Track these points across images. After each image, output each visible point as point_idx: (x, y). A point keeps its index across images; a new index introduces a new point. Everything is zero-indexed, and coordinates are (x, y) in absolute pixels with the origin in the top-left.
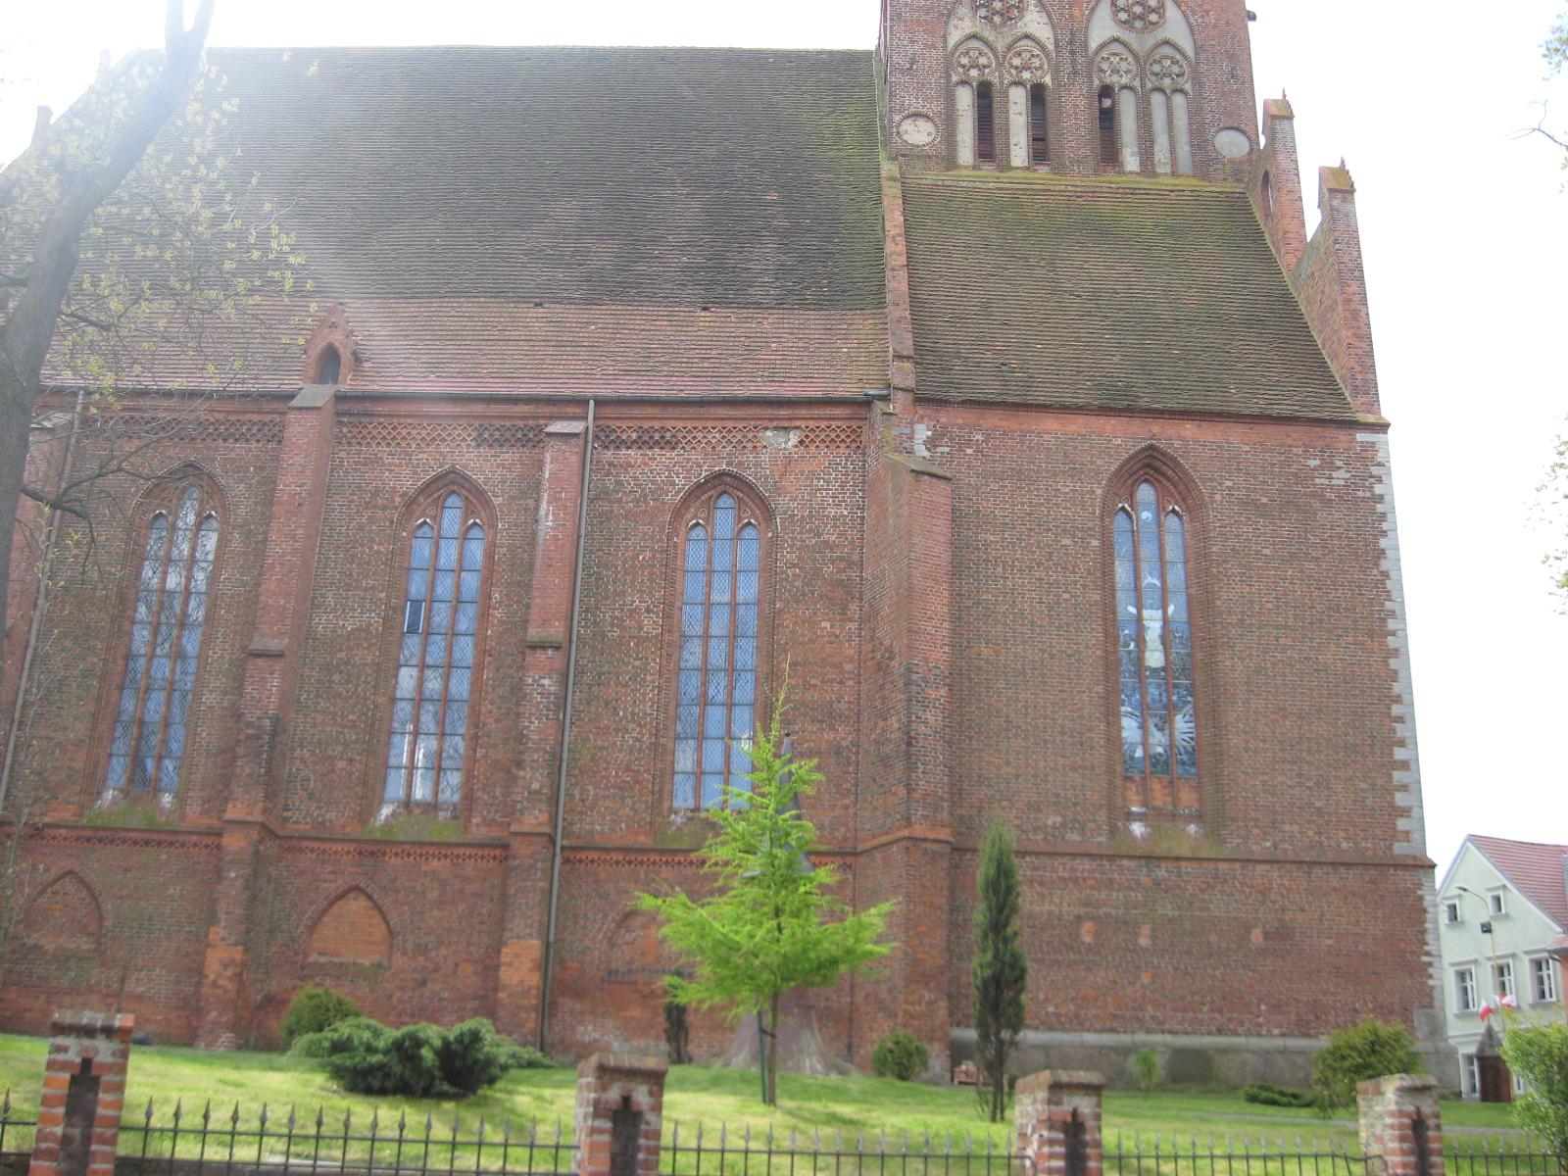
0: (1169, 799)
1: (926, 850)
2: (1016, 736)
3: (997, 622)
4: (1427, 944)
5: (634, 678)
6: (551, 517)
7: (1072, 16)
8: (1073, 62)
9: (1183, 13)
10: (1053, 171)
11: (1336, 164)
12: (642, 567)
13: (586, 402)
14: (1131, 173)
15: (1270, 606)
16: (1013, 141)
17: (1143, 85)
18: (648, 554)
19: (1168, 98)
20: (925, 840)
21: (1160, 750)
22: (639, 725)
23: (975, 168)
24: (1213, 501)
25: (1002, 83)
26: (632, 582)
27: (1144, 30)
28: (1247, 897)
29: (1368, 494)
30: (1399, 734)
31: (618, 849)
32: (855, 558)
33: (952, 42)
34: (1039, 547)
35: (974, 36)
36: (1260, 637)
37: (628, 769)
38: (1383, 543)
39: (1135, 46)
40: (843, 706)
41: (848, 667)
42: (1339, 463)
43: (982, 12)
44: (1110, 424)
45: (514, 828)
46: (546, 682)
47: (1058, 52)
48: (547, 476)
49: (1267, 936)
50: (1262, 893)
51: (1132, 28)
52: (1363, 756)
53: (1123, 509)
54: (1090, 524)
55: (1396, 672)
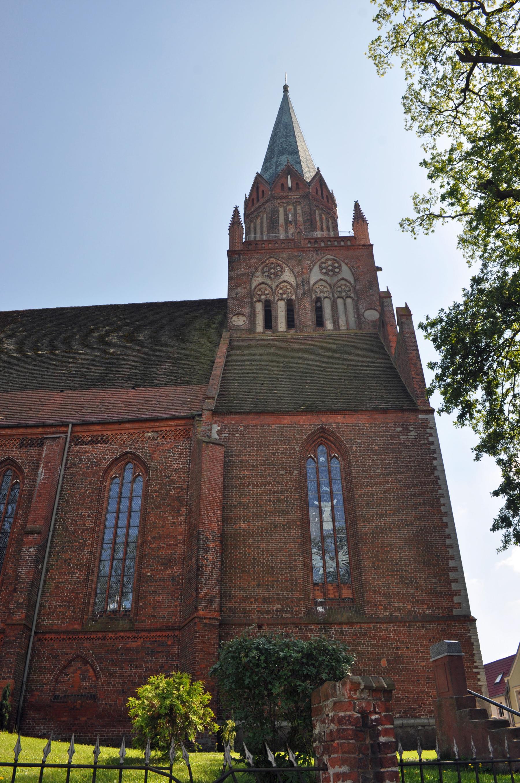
0: (337, 594)
1: (205, 623)
2: (258, 566)
3: (249, 511)
4: (475, 662)
5: (79, 548)
6: (43, 474)
7: (302, 272)
8: (304, 289)
9: (349, 267)
10: (296, 332)
11: (404, 306)
12: (88, 497)
13: (68, 425)
14: (329, 330)
15: (382, 496)
16: (279, 322)
17: (333, 296)
18: (91, 491)
19: (344, 300)
20: (205, 618)
21: (332, 569)
22: (80, 571)
23: (264, 333)
24: (352, 450)
25: (274, 300)
26: (83, 504)
27: (333, 275)
28: (377, 642)
29: (426, 442)
30: (451, 554)
31: (63, 632)
32: (185, 486)
33: (253, 286)
34: (269, 476)
35: (263, 283)
36: (377, 511)
37: (72, 592)
38: (435, 463)
39: (329, 282)
40: (176, 556)
41: (179, 537)
42: (411, 429)
43: (267, 274)
44: (302, 419)
45: (9, 621)
46: (32, 550)
47: (297, 286)
48: (43, 456)
49: (388, 661)
50: (385, 639)
51: (328, 275)
52: (433, 565)
53: (311, 457)
54: (294, 464)
55: (446, 523)
